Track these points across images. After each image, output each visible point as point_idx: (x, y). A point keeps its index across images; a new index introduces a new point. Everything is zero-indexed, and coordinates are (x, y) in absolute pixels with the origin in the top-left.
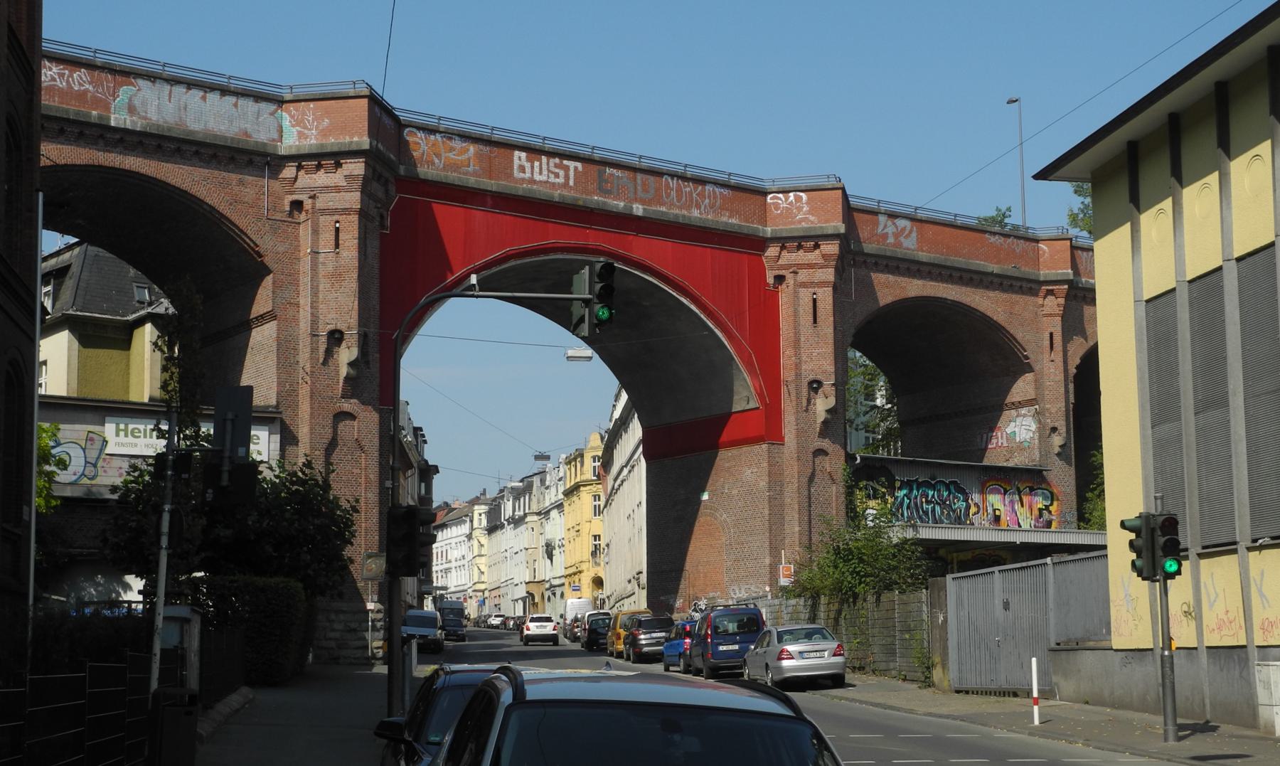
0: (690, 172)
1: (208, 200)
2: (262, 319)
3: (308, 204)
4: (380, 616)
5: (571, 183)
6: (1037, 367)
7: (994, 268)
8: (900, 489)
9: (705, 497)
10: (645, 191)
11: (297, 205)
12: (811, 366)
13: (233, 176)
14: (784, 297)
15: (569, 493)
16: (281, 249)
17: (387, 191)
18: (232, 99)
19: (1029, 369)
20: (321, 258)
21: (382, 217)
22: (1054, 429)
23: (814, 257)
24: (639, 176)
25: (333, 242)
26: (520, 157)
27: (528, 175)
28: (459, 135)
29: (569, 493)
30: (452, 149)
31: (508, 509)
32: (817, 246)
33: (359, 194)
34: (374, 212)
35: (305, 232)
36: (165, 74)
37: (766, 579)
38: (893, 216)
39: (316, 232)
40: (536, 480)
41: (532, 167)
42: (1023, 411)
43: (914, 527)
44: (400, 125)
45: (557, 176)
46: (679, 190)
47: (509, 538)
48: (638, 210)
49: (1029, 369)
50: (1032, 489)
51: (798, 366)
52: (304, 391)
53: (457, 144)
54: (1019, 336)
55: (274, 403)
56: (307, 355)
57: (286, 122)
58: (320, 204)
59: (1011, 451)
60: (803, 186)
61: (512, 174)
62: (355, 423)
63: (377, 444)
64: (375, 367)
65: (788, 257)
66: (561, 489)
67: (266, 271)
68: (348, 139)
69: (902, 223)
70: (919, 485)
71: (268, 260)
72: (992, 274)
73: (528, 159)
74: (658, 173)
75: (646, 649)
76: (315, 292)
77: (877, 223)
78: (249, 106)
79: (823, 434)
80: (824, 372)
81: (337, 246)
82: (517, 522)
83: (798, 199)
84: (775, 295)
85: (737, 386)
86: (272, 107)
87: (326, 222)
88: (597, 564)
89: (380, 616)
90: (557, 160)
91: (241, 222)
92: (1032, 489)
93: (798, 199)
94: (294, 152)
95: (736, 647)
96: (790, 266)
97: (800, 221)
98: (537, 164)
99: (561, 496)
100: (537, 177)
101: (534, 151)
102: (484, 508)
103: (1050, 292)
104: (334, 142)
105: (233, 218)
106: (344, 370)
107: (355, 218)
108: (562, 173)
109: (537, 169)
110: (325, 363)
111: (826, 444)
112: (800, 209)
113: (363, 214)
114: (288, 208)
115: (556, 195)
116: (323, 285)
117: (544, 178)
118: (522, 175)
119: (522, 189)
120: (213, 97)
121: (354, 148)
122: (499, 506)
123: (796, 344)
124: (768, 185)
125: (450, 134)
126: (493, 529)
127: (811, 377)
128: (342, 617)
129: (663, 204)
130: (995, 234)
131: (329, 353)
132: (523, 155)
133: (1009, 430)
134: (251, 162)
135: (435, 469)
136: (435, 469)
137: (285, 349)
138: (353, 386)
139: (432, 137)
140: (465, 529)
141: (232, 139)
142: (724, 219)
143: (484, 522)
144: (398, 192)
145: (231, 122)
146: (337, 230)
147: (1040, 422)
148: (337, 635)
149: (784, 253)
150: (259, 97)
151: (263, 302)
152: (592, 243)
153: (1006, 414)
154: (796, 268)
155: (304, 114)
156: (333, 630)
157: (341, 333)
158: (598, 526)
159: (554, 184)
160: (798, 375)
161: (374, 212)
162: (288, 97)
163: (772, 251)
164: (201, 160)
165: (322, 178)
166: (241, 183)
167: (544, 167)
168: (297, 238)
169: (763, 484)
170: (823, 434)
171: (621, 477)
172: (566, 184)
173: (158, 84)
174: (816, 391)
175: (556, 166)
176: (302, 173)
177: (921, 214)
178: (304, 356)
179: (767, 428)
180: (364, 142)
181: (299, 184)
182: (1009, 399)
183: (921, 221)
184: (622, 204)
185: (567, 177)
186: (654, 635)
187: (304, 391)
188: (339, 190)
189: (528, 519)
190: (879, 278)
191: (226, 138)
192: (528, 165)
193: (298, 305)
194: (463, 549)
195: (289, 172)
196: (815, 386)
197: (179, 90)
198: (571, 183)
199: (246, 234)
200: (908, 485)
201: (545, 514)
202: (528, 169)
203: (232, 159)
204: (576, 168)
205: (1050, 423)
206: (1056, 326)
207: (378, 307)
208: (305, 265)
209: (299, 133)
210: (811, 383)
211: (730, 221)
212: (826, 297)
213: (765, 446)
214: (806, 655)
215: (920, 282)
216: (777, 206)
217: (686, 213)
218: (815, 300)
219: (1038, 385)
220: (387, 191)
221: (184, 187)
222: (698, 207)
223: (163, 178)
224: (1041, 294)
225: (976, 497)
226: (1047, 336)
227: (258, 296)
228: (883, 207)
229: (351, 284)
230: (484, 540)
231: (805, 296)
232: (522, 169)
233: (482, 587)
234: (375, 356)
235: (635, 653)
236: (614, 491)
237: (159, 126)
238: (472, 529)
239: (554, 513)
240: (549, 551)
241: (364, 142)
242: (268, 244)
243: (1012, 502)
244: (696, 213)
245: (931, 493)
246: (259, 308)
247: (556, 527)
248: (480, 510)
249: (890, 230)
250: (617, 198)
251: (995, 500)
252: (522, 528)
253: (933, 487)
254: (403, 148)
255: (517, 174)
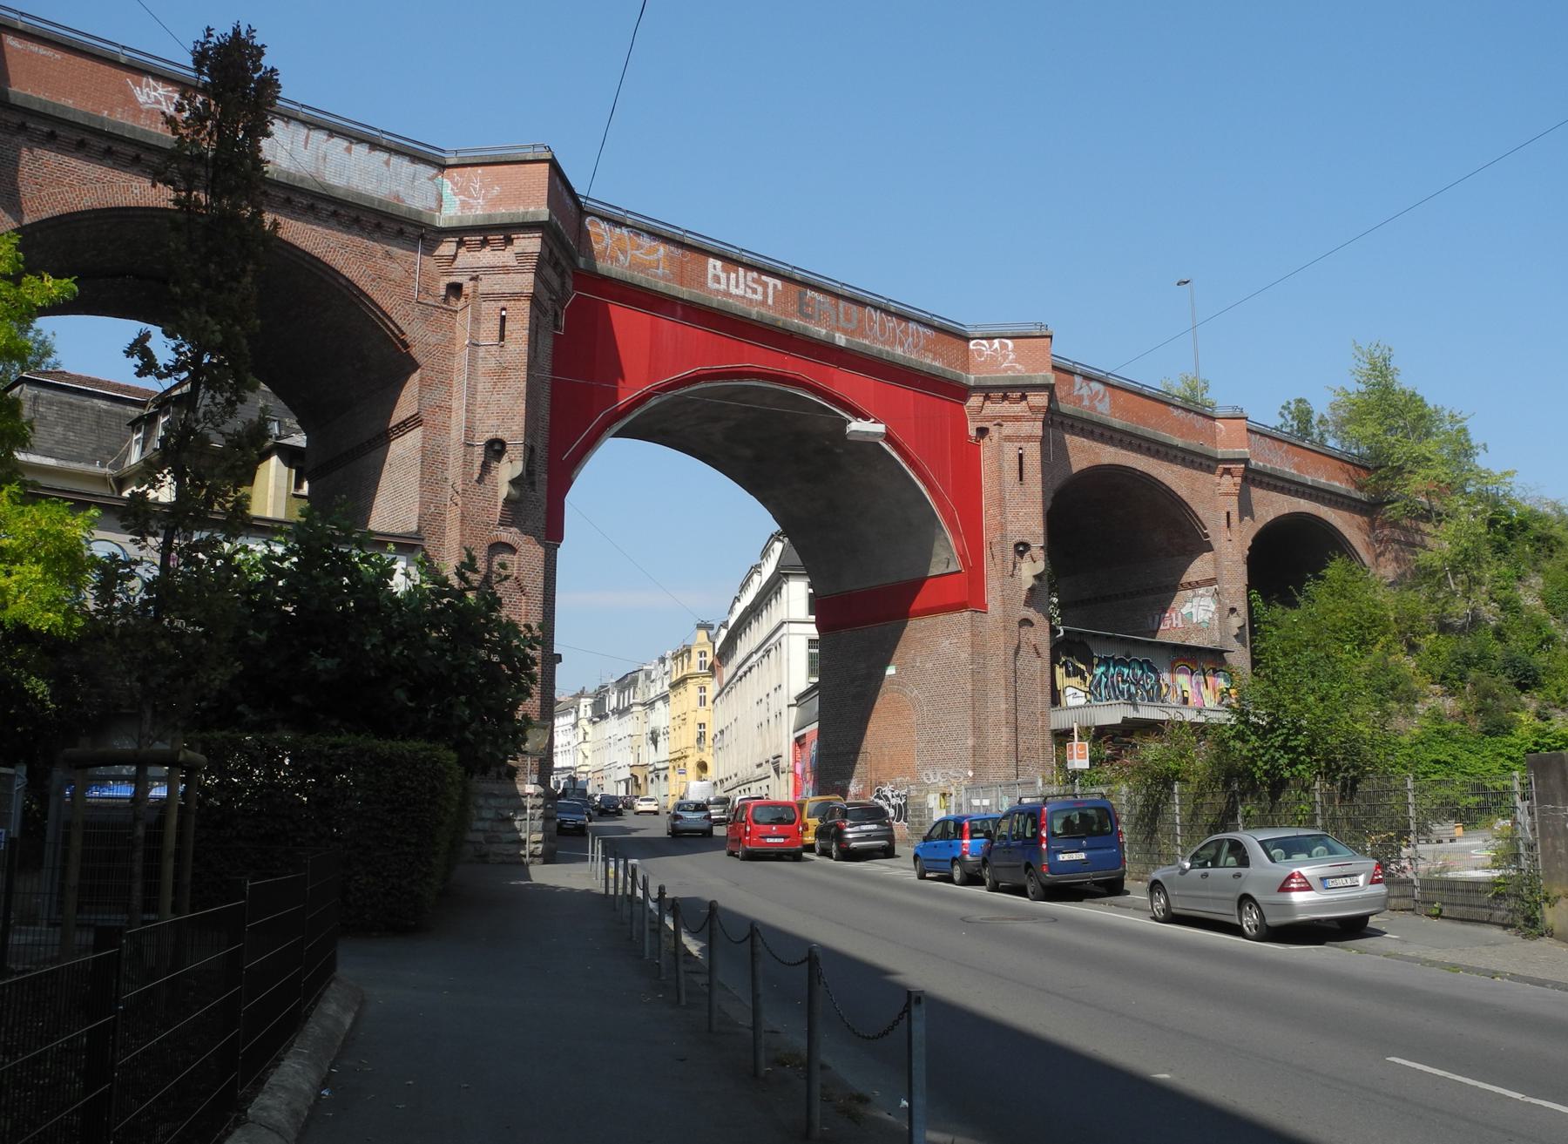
0: (893, 307)
1: (344, 272)
2: (405, 426)
3: (468, 287)
4: (540, 801)
5: (770, 301)
6: (1216, 546)
7: (1178, 441)
8: (1098, 666)
9: (891, 671)
10: (849, 320)
11: (455, 289)
12: (1016, 527)
13: (377, 246)
14: (987, 449)
15: (675, 686)
16: (432, 340)
17: (563, 285)
18: (384, 156)
19: (1209, 548)
20: (481, 352)
21: (556, 314)
22: (1233, 610)
23: (1019, 408)
24: (842, 304)
25: (497, 334)
26: (714, 265)
27: (723, 287)
28: (648, 233)
29: (675, 686)
30: (639, 247)
31: (612, 701)
32: (1024, 397)
33: (532, 276)
34: (548, 304)
35: (463, 321)
36: (301, 116)
37: (969, 763)
38: (1088, 378)
39: (476, 320)
40: (641, 676)
41: (728, 279)
42: (1201, 591)
43: (1135, 705)
44: (582, 212)
45: (755, 291)
46: (882, 324)
47: (612, 726)
48: (841, 340)
49: (1209, 548)
50: (1215, 671)
51: (1002, 526)
52: (452, 516)
53: (645, 241)
54: (1200, 513)
55: (415, 528)
56: (459, 470)
57: (448, 188)
58: (485, 285)
59: (1187, 632)
60: (1009, 331)
61: (703, 284)
62: (515, 558)
63: (541, 585)
64: (542, 491)
65: (992, 408)
66: (667, 682)
67: (415, 366)
68: (522, 209)
69: (1095, 386)
70: (1117, 663)
71: (415, 352)
72: (1176, 447)
73: (724, 270)
74: (862, 304)
75: (854, 845)
76: (472, 393)
77: (1072, 384)
78: (403, 166)
79: (1028, 603)
80: (1033, 533)
81: (502, 337)
82: (621, 712)
83: (1003, 346)
84: (976, 449)
85: (938, 548)
86: (432, 171)
87: (490, 309)
88: (701, 750)
89: (540, 801)
90: (755, 274)
91: (386, 303)
92: (1215, 671)
93: (1003, 346)
94: (455, 224)
95: (1082, 856)
96: (995, 418)
97: (1006, 370)
98: (733, 276)
99: (666, 688)
100: (733, 290)
101: (732, 261)
102: (589, 701)
103: (1227, 471)
104: (505, 212)
105: (375, 297)
106: (504, 490)
107: (526, 305)
108: (760, 289)
109: (733, 282)
110: (480, 480)
111: (1031, 613)
112: (1005, 357)
113: (534, 299)
114: (443, 292)
115: (754, 312)
116: (483, 385)
117: (740, 292)
118: (716, 286)
119: (715, 301)
120: (361, 150)
121: (529, 219)
122: (603, 699)
123: (1001, 502)
124: (970, 331)
125: (637, 230)
126: (599, 714)
127: (1018, 539)
128: (492, 802)
129: (865, 337)
130: (1178, 407)
131: (485, 468)
132: (719, 264)
133: (1184, 611)
134: (401, 232)
135: (559, 658)
136: (559, 658)
137: (431, 462)
138: (514, 511)
139: (618, 230)
140: (571, 719)
141: (380, 201)
142: (928, 361)
143: (589, 713)
144: (576, 288)
145: (380, 182)
146: (503, 319)
147: (1219, 602)
148: (487, 825)
149: (988, 403)
150: (416, 157)
151: (406, 405)
152: (790, 371)
153: (1181, 595)
154: (1000, 421)
155: (470, 180)
156: (483, 819)
157: (502, 443)
158: (703, 715)
159: (751, 300)
160: (1003, 536)
161: (548, 304)
162: (451, 161)
163: (975, 401)
164: (340, 223)
165: (487, 257)
166: (388, 255)
167: (741, 280)
168: (452, 329)
169: (964, 656)
170: (1028, 603)
171: (749, 664)
172: (764, 303)
173: (293, 126)
174: (1021, 554)
175: (754, 281)
176: (463, 250)
177: (1113, 380)
178: (454, 472)
179: (967, 595)
180: (542, 212)
181: (459, 263)
182: (1185, 579)
183: (1113, 386)
184: (824, 331)
185: (765, 294)
186: (864, 828)
187: (452, 516)
188: (509, 271)
189: (634, 709)
190: (1073, 442)
191: (372, 199)
192: (723, 276)
193: (450, 409)
194: (570, 737)
195: (447, 248)
196: (1022, 548)
197: (318, 136)
198: (770, 301)
199: (390, 319)
200: (1105, 662)
201: (650, 705)
202: (723, 281)
203: (379, 226)
204: (775, 286)
205: (1229, 604)
206: (1233, 505)
207: (547, 418)
208: (461, 359)
209: (463, 202)
210: (1016, 546)
211: (932, 362)
212: (1033, 452)
213: (966, 614)
214: (1330, 883)
215: (1112, 449)
216: (980, 353)
217: (887, 348)
218: (1021, 456)
219: (1216, 563)
220: (563, 285)
221: (317, 252)
222: (902, 344)
223: (291, 240)
224: (1218, 472)
225: (1166, 677)
226: (1224, 515)
227: (401, 399)
228: (1079, 368)
229: (519, 383)
230: (589, 729)
231: (1011, 451)
232: (717, 279)
233: (586, 769)
234: (542, 477)
235: (839, 849)
236: (738, 678)
237: (289, 174)
238: (578, 719)
239: (659, 704)
240: (654, 738)
241: (542, 212)
242: (418, 333)
243: (1198, 683)
244: (899, 351)
245: (1126, 671)
246: (400, 413)
247: (661, 717)
248: (585, 703)
249: (1085, 392)
250: (819, 324)
251: (1183, 680)
252: (626, 718)
253: (1128, 665)
254: (583, 235)
255: (711, 284)
